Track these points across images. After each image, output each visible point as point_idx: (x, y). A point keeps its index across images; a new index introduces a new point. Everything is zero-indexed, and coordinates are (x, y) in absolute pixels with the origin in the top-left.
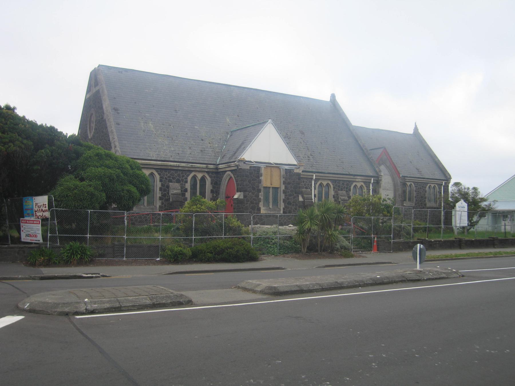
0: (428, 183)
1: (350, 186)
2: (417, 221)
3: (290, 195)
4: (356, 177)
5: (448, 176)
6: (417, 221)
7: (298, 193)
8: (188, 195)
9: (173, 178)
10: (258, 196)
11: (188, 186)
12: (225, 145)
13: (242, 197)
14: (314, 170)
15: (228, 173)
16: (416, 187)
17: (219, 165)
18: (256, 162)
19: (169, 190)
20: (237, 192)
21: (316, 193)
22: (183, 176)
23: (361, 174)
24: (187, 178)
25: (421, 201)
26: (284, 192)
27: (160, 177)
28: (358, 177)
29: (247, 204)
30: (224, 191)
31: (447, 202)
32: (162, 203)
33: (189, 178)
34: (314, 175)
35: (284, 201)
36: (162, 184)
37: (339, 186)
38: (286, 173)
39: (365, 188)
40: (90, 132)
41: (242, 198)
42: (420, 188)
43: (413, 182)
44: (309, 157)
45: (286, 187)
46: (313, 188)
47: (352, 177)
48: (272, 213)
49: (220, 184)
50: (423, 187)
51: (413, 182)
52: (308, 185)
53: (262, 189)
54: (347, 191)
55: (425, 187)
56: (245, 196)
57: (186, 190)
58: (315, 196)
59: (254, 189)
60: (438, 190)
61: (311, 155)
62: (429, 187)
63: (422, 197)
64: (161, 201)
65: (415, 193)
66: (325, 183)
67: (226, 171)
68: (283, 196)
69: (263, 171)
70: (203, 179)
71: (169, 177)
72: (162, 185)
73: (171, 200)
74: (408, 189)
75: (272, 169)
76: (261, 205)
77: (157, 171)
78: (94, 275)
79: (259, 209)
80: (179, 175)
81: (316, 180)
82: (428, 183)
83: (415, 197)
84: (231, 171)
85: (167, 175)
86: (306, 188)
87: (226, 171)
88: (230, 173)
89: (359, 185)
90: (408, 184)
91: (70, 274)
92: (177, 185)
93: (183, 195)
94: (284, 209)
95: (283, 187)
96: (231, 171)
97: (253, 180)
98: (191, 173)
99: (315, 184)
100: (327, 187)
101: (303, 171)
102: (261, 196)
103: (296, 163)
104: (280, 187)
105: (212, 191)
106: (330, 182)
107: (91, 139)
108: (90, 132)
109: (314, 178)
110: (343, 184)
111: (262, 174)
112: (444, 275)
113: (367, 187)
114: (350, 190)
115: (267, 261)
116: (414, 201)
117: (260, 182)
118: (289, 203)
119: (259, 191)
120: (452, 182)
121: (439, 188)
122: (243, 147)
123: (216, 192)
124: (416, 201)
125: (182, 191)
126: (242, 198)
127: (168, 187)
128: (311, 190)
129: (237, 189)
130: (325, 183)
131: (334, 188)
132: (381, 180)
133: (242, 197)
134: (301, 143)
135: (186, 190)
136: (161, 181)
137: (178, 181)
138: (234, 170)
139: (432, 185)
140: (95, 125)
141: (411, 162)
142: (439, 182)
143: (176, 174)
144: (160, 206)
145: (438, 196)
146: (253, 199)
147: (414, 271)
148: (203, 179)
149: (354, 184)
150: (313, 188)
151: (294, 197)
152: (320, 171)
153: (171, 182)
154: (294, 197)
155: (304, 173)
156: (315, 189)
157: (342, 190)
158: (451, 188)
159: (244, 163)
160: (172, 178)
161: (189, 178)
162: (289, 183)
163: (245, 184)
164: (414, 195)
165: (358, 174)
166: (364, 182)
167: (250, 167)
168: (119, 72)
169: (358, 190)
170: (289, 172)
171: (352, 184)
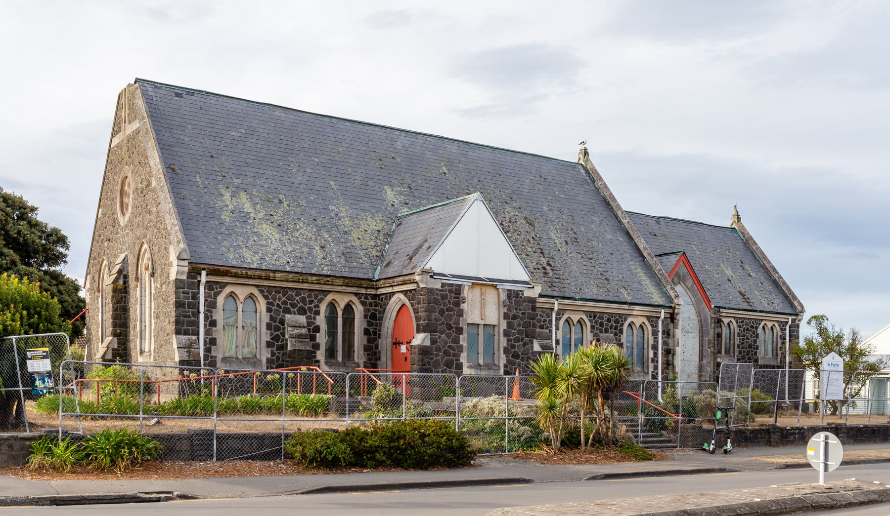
0: (762, 320)
1: (622, 325)
2: (757, 391)
3: (517, 340)
4: (632, 307)
5: (799, 308)
6: (757, 391)
7: (532, 336)
8: (322, 338)
9: (294, 305)
10: (456, 340)
11: (321, 321)
12: (389, 243)
13: (428, 343)
14: (555, 294)
15: (396, 296)
16: (739, 327)
17: (377, 281)
18: (453, 276)
19: (284, 329)
20: (418, 332)
21: (560, 337)
22: (311, 302)
23: (642, 302)
24: (318, 306)
25: (748, 354)
26: (506, 334)
27: (268, 303)
28: (637, 308)
29: (437, 355)
30: (390, 331)
31: (798, 355)
32: (273, 354)
33: (323, 308)
34: (556, 302)
35: (506, 351)
36: (271, 316)
37: (601, 325)
38: (509, 297)
39: (650, 328)
40: (123, 214)
41: (429, 344)
42: (748, 330)
43: (734, 318)
44: (544, 268)
45: (509, 325)
46: (554, 327)
47: (626, 307)
48: (483, 373)
49: (381, 319)
50: (752, 327)
51: (734, 318)
52: (545, 321)
53: (465, 327)
54: (616, 334)
55: (757, 328)
56: (433, 341)
57: (317, 329)
58: (557, 342)
59: (450, 327)
60: (780, 333)
61: (549, 265)
62: (763, 327)
63: (750, 346)
64: (270, 350)
65: (737, 338)
66: (575, 318)
67: (393, 293)
68: (503, 342)
69: (466, 292)
70: (348, 309)
71: (285, 303)
72: (272, 318)
73: (289, 348)
74: (725, 331)
75: (484, 288)
76: (463, 358)
77: (261, 292)
78: (162, 496)
79: (460, 367)
80: (303, 300)
81: (560, 313)
82: (762, 320)
83: (738, 346)
84: (405, 293)
85: (280, 299)
86: (542, 327)
87: (393, 293)
88: (402, 296)
89: (638, 321)
90: (726, 321)
91: (112, 494)
92: (302, 319)
93: (313, 338)
94: (505, 366)
95: (504, 325)
96: (405, 293)
97: (448, 310)
98: (325, 296)
99: (558, 319)
100: (579, 325)
101: (541, 296)
102: (463, 340)
103: (525, 277)
104: (499, 325)
105: (366, 332)
106: (584, 317)
107: (126, 226)
108: (123, 214)
109: (556, 308)
110: (609, 320)
111: (464, 299)
112: (875, 497)
113: (652, 326)
114: (621, 332)
115: (490, 467)
116: (736, 354)
117: (461, 314)
118: (516, 356)
119: (460, 331)
120: (806, 317)
121: (782, 329)
122: (426, 245)
123: (375, 333)
124: (740, 353)
125: (309, 330)
126: (429, 344)
127: (282, 322)
128: (550, 331)
129: (418, 326)
130: (575, 318)
131: (593, 327)
132: (678, 314)
133: (428, 343)
134: (529, 241)
135: (317, 329)
136: (269, 310)
137: (302, 312)
138: (410, 291)
139: (770, 324)
140: (134, 199)
141: (729, 280)
142: (782, 318)
143: (297, 298)
144: (268, 359)
145: (779, 345)
146: (449, 347)
147: (815, 488)
148: (348, 309)
149: (629, 320)
150: (554, 327)
151: (525, 344)
152: (567, 295)
153: (290, 313)
154: (525, 344)
155: (541, 300)
156: (557, 329)
157: (606, 331)
158: (807, 332)
159: (431, 277)
160: (291, 304)
161: (323, 308)
162: (515, 317)
163: (433, 317)
164: (737, 343)
165: (638, 302)
166: (648, 318)
167: (443, 285)
168: (177, 95)
169: (635, 332)
170: (514, 298)
171: (626, 320)
